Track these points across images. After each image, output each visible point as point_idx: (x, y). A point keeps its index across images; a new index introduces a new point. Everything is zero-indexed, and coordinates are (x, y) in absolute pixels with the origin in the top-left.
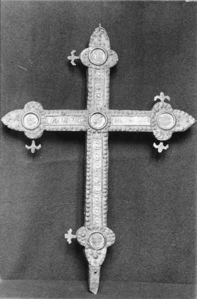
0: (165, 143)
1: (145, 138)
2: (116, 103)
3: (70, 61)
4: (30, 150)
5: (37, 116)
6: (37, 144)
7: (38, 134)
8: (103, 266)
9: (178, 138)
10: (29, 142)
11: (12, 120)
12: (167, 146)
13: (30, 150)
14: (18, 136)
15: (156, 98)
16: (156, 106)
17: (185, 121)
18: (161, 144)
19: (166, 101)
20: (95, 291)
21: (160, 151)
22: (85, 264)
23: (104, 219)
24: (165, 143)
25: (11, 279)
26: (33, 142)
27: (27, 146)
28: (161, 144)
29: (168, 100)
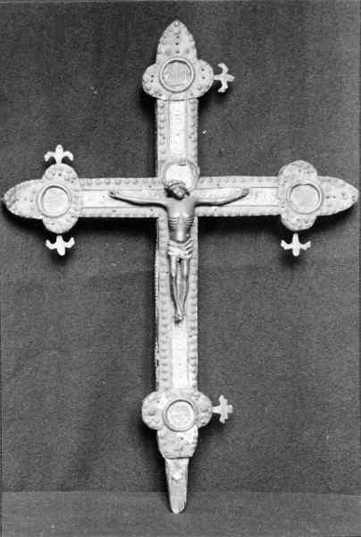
0: (66, 237)
1: (271, 226)
2: (210, 162)
3: (229, 73)
4: (291, 251)
5: (61, 188)
6: (302, 241)
7: (66, 224)
8: (193, 462)
9: (326, 224)
10: (52, 237)
11: (24, 201)
12: (72, 242)
13: (291, 251)
14: (35, 228)
15: (47, 157)
16: (48, 172)
17: (340, 196)
18: (59, 239)
19: (65, 160)
20: (176, 510)
21: (62, 252)
22: (160, 463)
23: (191, 381)
24: (66, 237)
25: (62, 490)
26: (296, 237)
27: (283, 244)
28: (59, 239)
29: (69, 160)
